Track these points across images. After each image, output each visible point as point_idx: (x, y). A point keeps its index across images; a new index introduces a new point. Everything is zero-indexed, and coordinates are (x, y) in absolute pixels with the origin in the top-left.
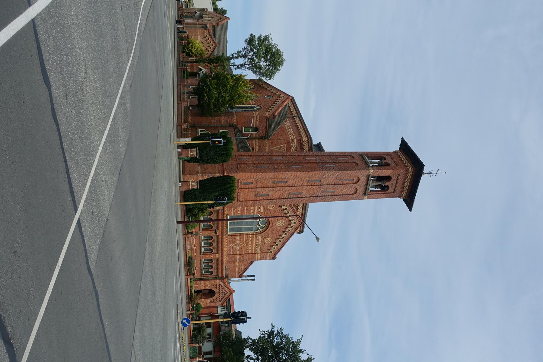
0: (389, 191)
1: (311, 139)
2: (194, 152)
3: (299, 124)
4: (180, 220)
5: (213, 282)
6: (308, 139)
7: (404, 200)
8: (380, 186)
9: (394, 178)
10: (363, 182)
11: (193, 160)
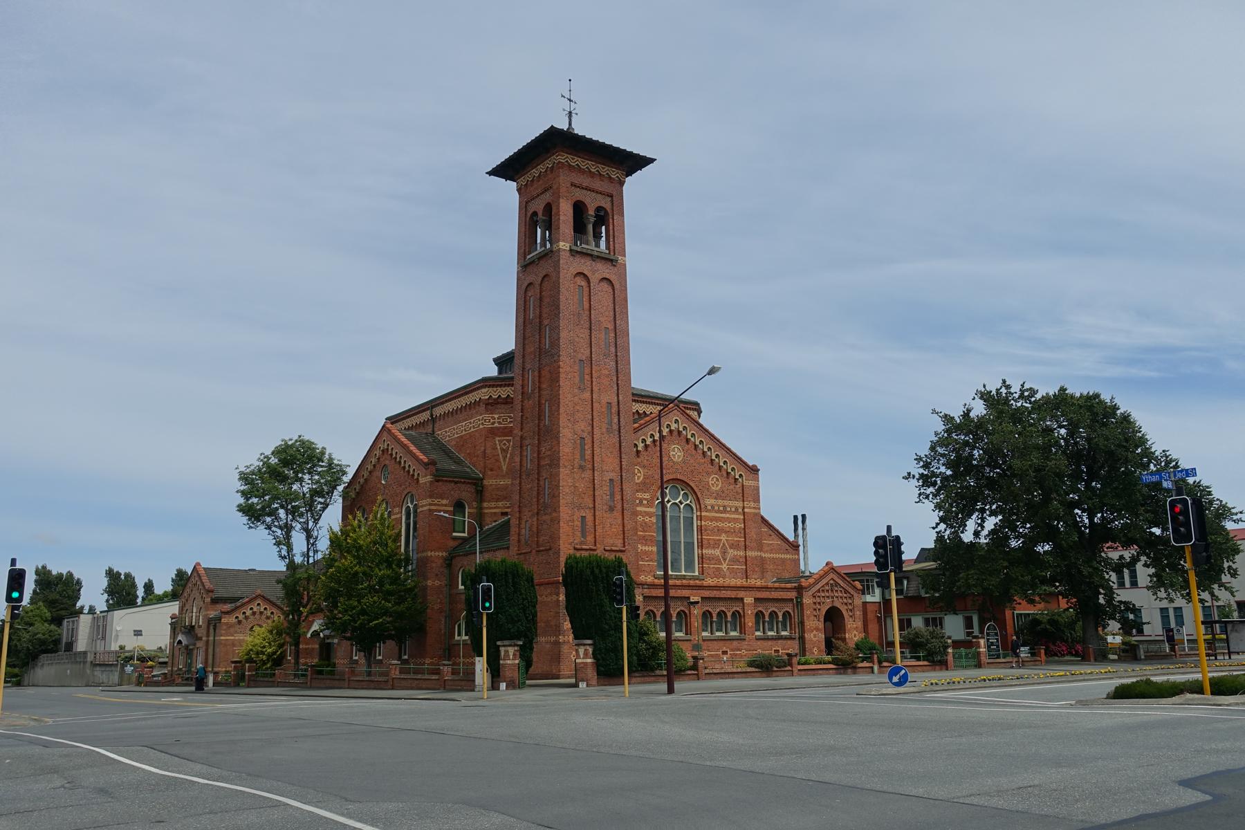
0: (608, 206)
3: (449, 406)
5: (807, 612)
8: (597, 226)
10: (585, 266)
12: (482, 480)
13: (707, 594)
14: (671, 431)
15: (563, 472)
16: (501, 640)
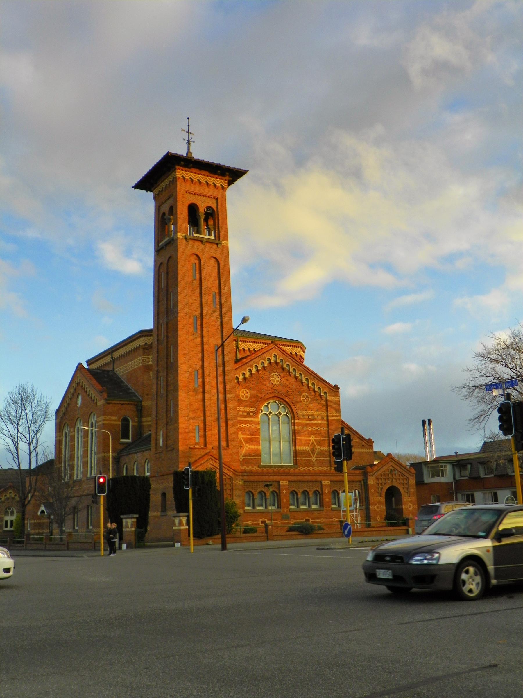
0: (214, 206)
1: (142, 332)
2: (127, 522)
3: (122, 351)
4: (220, 546)
5: (372, 490)
6: (143, 336)
7: (230, 183)
8: (206, 220)
9: (193, 199)
10: (197, 248)
11: (142, 523)
12: (141, 402)
13: (293, 478)
14: (270, 363)
15: (181, 395)
16: (123, 514)
